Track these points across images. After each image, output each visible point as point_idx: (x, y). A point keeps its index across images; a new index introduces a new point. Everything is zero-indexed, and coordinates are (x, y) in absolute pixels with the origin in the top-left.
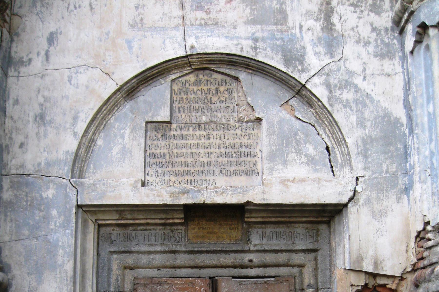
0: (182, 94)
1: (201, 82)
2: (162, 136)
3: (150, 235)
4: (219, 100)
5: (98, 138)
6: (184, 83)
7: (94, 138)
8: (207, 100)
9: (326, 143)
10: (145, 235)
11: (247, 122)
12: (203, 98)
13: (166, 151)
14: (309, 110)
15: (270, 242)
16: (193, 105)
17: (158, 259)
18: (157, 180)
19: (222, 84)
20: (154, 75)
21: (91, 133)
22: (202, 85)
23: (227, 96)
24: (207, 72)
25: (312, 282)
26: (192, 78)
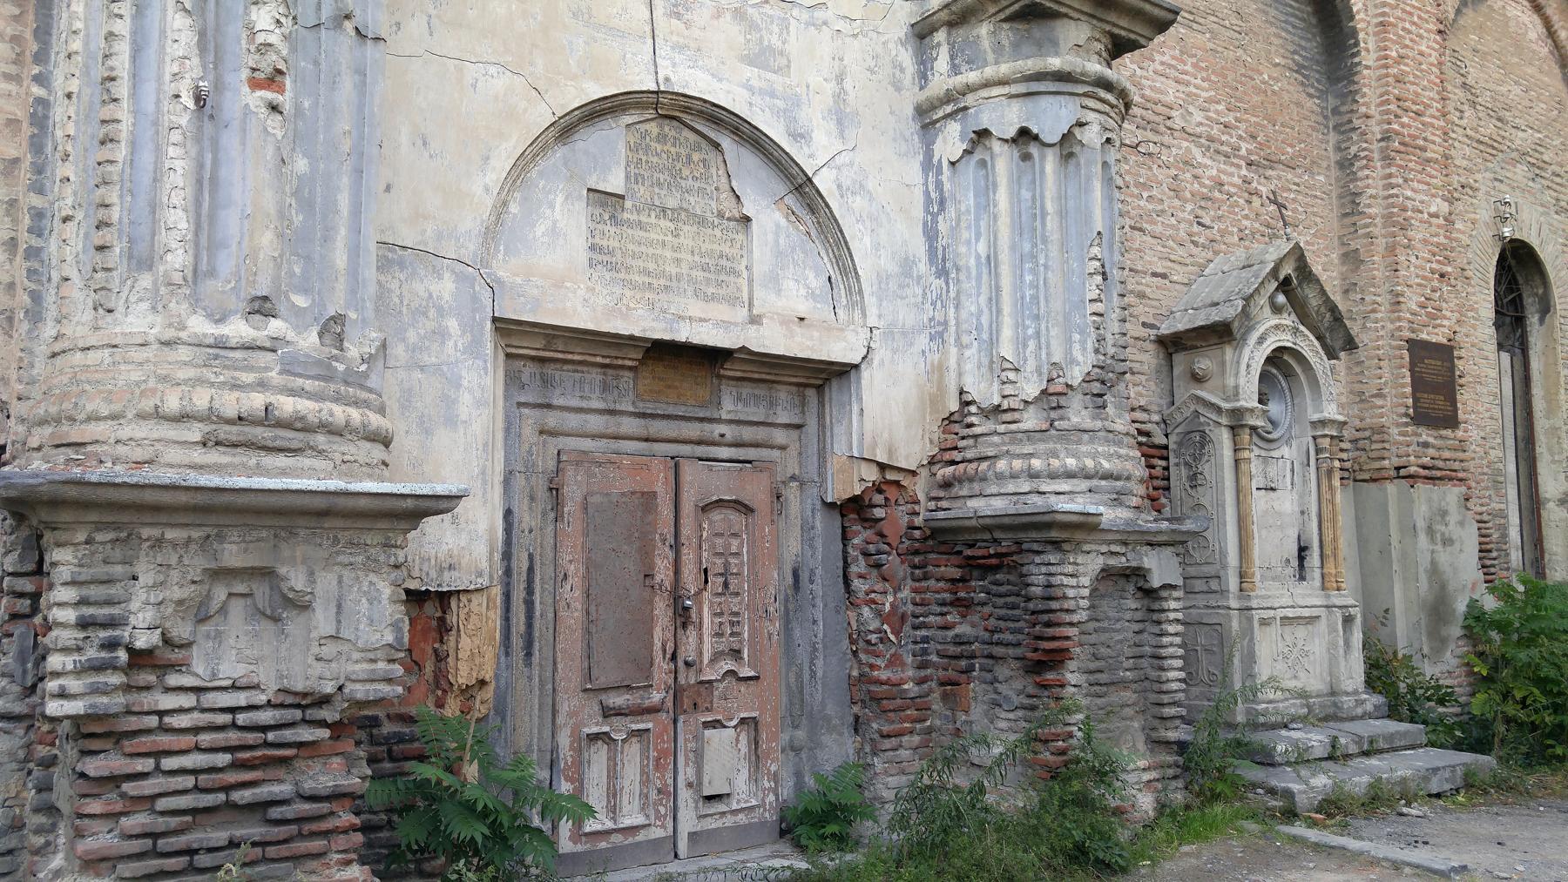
2: (610, 218)
13: (616, 244)
15: (746, 409)
16: (656, 175)
17: (596, 423)
18: (605, 292)
24: (675, 123)
26: (653, 128)
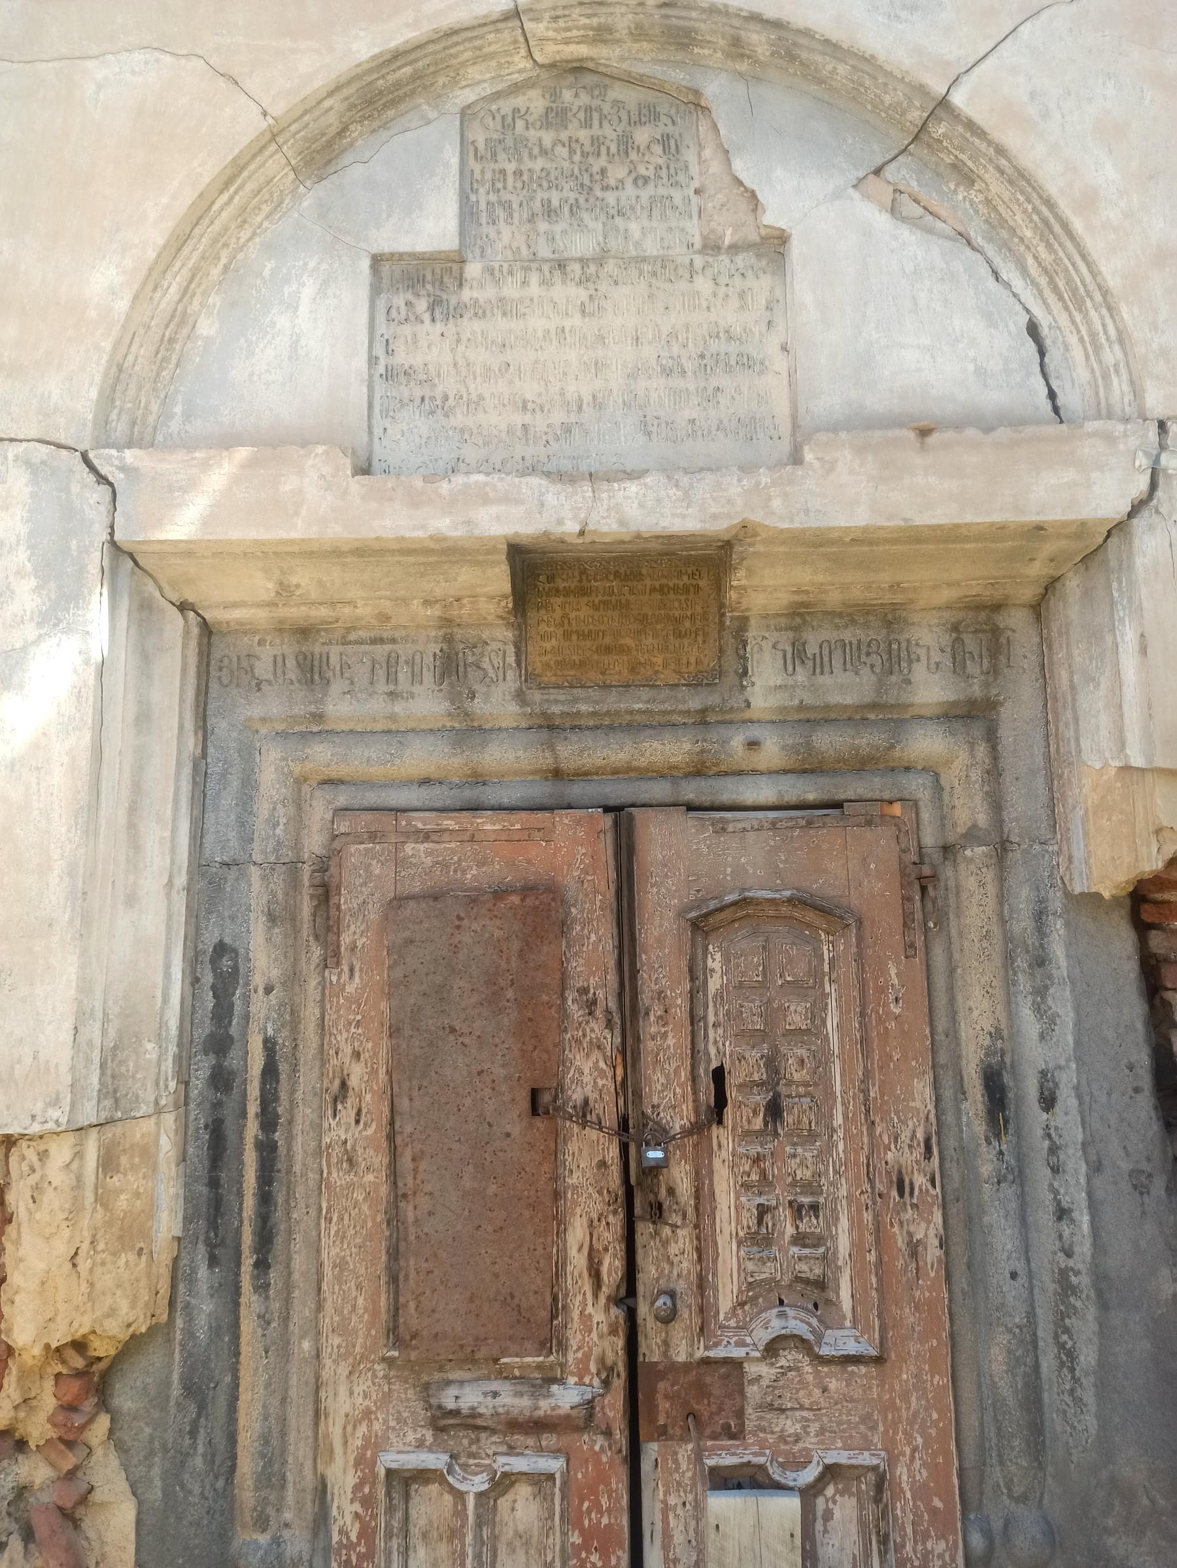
0: (502, 156)
1: (569, 114)
2: (431, 309)
3: (392, 660)
4: (634, 175)
5: (200, 312)
6: (510, 119)
7: (184, 313)
8: (591, 175)
9: (1028, 311)
10: (374, 662)
11: (734, 248)
12: (576, 171)
14: (960, 197)
16: (540, 195)
19: (643, 119)
20: (398, 85)
21: (173, 289)
22: (570, 126)
23: (661, 161)
25: (982, 819)
